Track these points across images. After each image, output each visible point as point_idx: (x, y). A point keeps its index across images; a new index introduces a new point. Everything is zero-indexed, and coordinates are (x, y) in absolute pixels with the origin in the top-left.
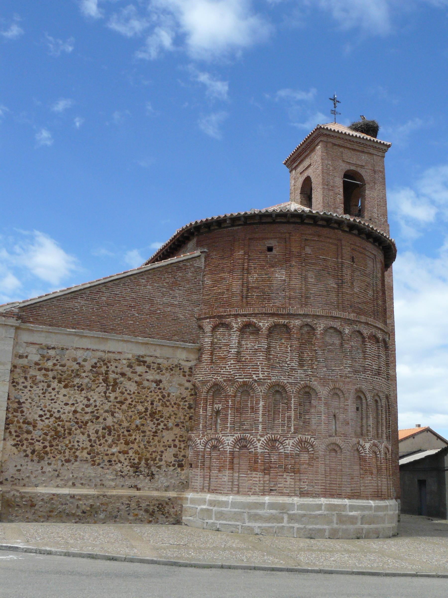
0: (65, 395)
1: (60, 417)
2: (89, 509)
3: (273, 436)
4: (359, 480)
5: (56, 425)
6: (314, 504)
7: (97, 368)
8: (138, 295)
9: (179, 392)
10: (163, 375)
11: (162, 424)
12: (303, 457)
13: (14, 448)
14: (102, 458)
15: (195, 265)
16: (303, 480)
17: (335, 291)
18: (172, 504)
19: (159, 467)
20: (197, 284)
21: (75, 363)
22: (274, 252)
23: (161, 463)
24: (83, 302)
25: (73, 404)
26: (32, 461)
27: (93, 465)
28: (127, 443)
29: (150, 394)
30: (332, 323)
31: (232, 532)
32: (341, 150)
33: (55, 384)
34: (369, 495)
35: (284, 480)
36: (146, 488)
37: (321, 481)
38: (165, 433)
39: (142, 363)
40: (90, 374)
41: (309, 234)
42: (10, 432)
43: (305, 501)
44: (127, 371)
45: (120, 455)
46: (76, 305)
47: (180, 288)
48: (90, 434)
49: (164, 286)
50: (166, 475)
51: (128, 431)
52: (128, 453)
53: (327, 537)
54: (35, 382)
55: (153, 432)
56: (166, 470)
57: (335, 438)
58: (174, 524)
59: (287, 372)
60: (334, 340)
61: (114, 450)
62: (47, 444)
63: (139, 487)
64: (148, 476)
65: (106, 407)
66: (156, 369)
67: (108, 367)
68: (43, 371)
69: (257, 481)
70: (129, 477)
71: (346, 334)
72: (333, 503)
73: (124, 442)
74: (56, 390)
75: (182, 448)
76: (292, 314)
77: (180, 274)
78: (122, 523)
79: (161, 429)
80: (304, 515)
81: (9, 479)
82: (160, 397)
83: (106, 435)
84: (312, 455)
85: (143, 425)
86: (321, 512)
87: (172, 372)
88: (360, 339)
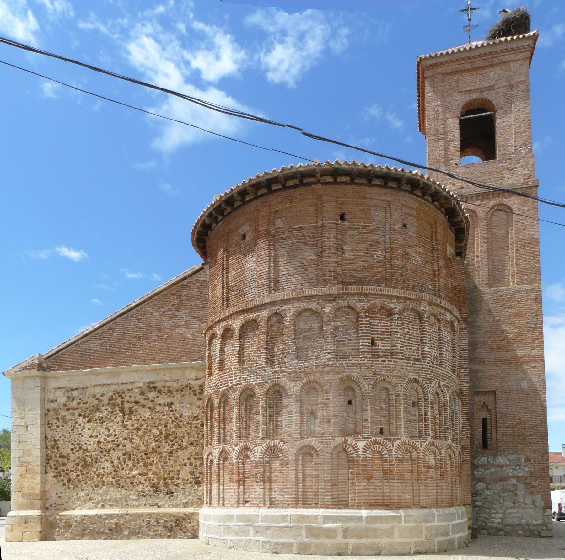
0: (89, 429)
1: (87, 449)
2: (114, 526)
3: (245, 444)
4: (346, 486)
5: (84, 456)
7: (113, 401)
8: (145, 324)
10: (174, 397)
13: (54, 479)
14: (125, 481)
15: (200, 279)
17: (314, 264)
18: (189, 519)
19: (177, 485)
20: (203, 299)
21: (94, 399)
24: (97, 343)
25: (97, 436)
26: (69, 488)
27: (117, 488)
28: (146, 466)
29: (163, 417)
30: (305, 305)
33: (80, 420)
35: (254, 490)
37: (292, 490)
38: (180, 453)
39: (153, 389)
40: (108, 407)
42: (50, 466)
45: (140, 477)
46: (92, 346)
47: (186, 307)
48: (113, 460)
49: (170, 309)
50: (184, 493)
51: (146, 454)
52: (147, 475)
54: (65, 422)
55: (169, 453)
56: (184, 487)
57: (308, 439)
59: (255, 372)
60: (312, 324)
61: (135, 472)
62: (79, 473)
63: (159, 504)
64: (168, 494)
65: (125, 435)
66: (166, 393)
67: (123, 398)
68: (71, 411)
70: (150, 496)
71: (325, 313)
73: (143, 465)
74: (82, 425)
75: (198, 466)
77: (185, 293)
78: (144, 538)
79: (176, 449)
80: (268, 528)
81: (53, 505)
82: (173, 418)
83: (127, 460)
85: (159, 447)
86: (286, 524)
87: (182, 393)
88: (352, 316)
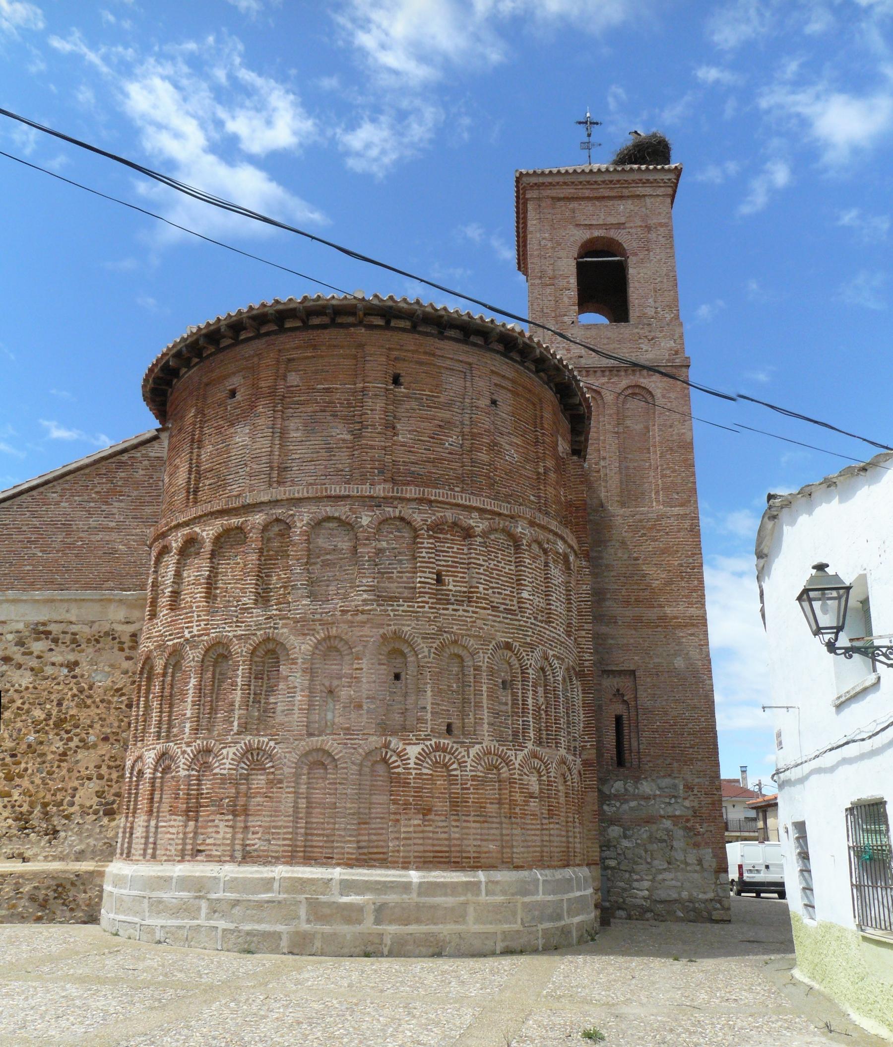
4: (385, 826)
6: (257, 879)
9: (110, 679)
11: (76, 739)
12: (255, 782)
15: (152, 454)
16: (252, 829)
18: (83, 884)
19: (67, 817)
22: (238, 397)
23: (72, 810)
29: (56, 687)
30: (329, 510)
31: (130, 938)
32: (571, 206)
34: (412, 859)
36: (40, 858)
39: (43, 636)
41: (294, 349)
43: (241, 872)
44: (14, 653)
51: (13, 756)
52: (10, 796)
53: (285, 950)
58: (85, 923)
59: (234, 616)
63: (26, 855)
64: (46, 835)
66: (68, 643)
69: (173, 834)
70: (10, 838)
71: (362, 526)
72: (300, 875)
76: (249, 505)
77: (123, 475)
80: (236, 903)
82: (75, 691)
84: (272, 777)
85: (41, 743)
87: (98, 646)
88: (407, 534)
